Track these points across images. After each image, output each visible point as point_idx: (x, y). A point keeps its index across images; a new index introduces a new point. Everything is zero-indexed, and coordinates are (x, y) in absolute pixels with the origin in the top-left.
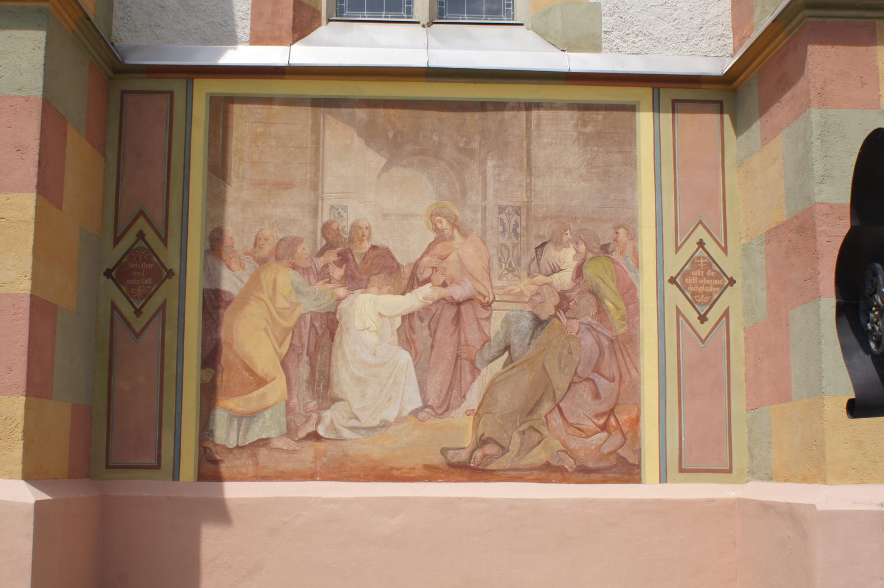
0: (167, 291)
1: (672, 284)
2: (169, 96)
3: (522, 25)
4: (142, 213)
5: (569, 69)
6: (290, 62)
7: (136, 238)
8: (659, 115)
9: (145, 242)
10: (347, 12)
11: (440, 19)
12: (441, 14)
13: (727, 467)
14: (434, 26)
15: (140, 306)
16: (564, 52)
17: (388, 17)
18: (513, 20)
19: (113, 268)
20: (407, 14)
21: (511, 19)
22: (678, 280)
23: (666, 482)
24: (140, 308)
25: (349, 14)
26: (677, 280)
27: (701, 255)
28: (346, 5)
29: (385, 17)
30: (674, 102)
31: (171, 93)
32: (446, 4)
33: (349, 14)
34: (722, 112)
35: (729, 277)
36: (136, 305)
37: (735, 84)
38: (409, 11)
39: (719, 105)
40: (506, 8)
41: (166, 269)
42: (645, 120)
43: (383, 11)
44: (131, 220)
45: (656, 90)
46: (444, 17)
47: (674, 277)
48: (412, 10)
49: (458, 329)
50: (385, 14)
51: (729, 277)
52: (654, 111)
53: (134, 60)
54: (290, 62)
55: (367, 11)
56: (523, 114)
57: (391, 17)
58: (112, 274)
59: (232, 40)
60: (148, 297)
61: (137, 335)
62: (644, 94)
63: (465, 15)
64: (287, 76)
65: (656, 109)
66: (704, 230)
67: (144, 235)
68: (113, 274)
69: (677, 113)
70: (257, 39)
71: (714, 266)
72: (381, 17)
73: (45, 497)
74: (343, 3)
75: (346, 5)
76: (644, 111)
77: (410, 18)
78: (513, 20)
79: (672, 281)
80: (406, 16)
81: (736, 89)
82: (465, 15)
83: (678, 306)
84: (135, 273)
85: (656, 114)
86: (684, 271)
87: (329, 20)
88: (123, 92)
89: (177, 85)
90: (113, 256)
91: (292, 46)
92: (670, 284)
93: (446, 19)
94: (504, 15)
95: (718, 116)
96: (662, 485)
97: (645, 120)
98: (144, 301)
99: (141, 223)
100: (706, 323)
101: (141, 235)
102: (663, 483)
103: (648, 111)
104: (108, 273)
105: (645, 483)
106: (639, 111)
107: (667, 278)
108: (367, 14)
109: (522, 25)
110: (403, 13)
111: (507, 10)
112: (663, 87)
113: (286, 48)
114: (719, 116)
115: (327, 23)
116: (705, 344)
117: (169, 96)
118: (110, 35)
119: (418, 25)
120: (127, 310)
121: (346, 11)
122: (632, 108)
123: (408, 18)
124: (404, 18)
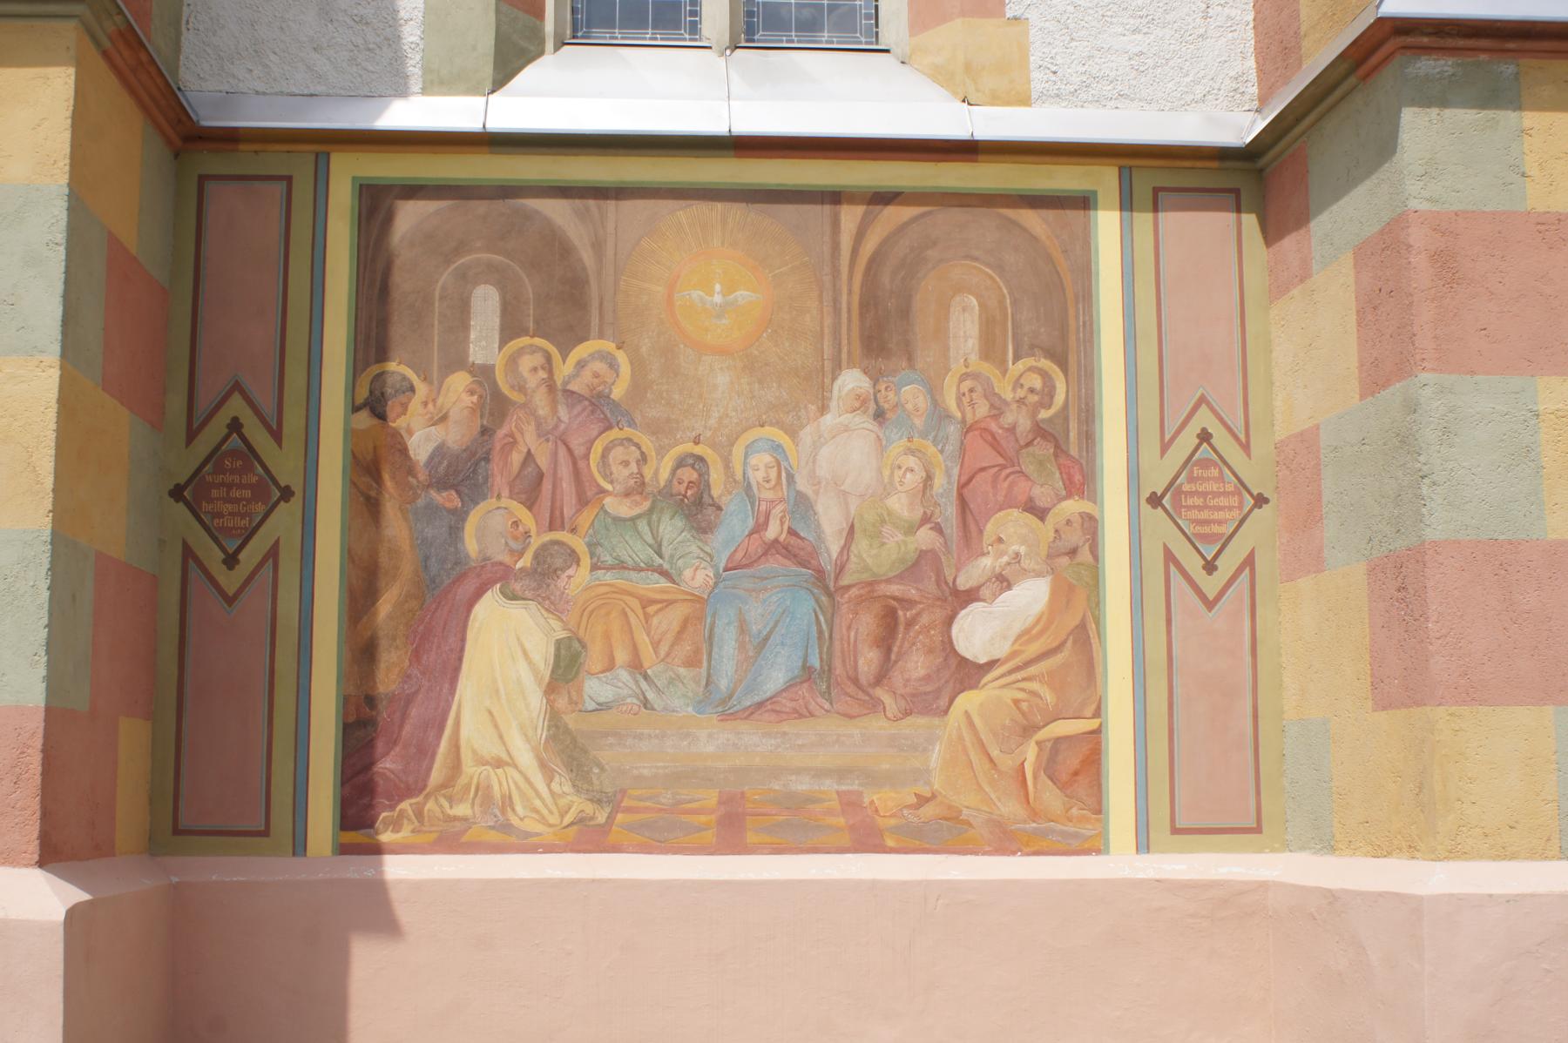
0: (283, 522)
1: (1155, 507)
2: (285, 183)
3: (887, 51)
4: (237, 387)
5: (484, 126)
7: (1197, 441)
8: (1132, 215)
9: (1211, 445)
10: (761, 33)
12: (750, 31)
17: (656, 39)
18: (877, 43)
19: (185, 483)
20: (690, 34)
21: (874, 40)
25: (764, 35)
26: (1252, 502)
27: (1205, 456)
28: (582, 17)
29: (651, 39)
32: (758, 14)
33: (764, 35)
34: (1239, 210)
37: (1262, 162)
38: (694, 28)
39: (1234, 195)
40: (688, 19)
41: (276, 483)
42: (1107, 223)
43: (822, 31)
45: (1126, 173)
47: (183, 483)
48: (699, 26)
49: (951, 585)
50: (652, 34)
52: (1121, 209)
53: (211, 119)
54: (487, 126)
56: (827, 208)
57: (662, 39)
58: (185, 494)
61: (230, 600)
62: (1105, 179)
63: (793, 34)
64: (980, 157)
65: (1127, 204)
66: (1210, 414)
67: (241, 426)
68: (1166, 501)
69: (1162, 211)
70: (438, 83)
71: (1228, 476)
72: (645, 39)
74: (754, 17)
77: (695, 40)
78: (877, 43)
79: (287, 494)
81: (1261, 170)
83: (1170, 546)
84: (215, 493)
85: (1126, 214)
86: (1175, 485)
87: (560, 43)
88: (203, 179)
89: (300, 167)
90: (184, 465)
91: (490, 96)
92: (1149, 506)
94: (685, 31)
95: (1233, 216)
97: (1107, 223)
99: (236, 406)
100: (1215, 573)
101: (235, 426)
104: (177, 493)
106: (1096, 209)
107: (1146, 494)
108: (620, 33)
109: (710, 48)
110: (683, 32)
115: (557, 49)
116: (1213, 611)
117: (285, 183)
118: (175, 71)
119: (888, 54)
120: (212, 556)
121: (758, 32)
122: (1084, 202)
123: (691, 40)
124: (685, 40)
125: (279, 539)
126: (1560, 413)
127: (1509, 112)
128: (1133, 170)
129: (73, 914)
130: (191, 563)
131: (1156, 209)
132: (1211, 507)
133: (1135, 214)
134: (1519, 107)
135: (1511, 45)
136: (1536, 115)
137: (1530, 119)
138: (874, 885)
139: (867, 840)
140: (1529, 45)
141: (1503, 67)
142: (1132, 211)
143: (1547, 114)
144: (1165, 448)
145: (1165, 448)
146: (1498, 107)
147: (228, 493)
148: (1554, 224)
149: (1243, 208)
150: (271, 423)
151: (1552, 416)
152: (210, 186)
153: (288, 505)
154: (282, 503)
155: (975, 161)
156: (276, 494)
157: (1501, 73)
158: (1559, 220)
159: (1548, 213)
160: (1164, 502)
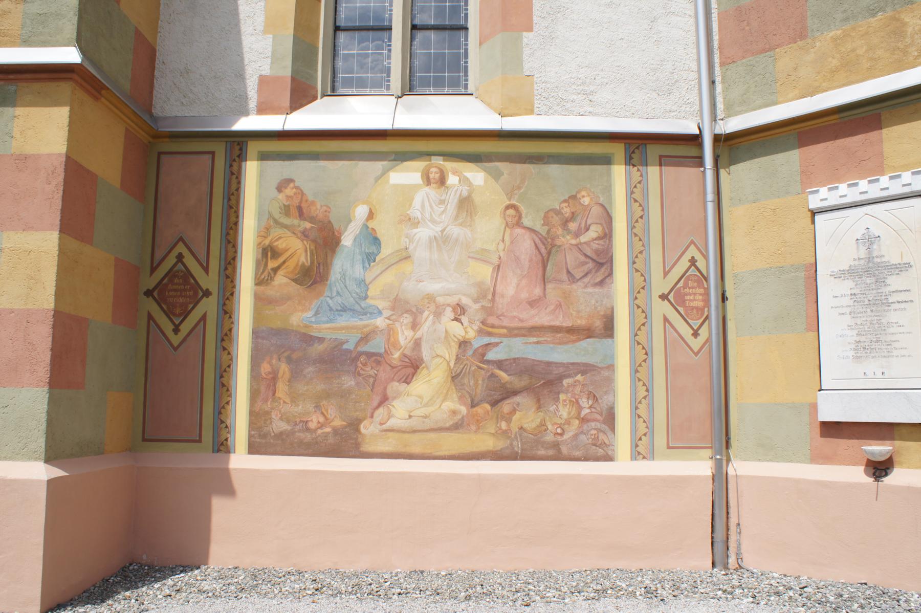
1: (663, 300)
3: (472, 94)
6: (503, 128)
11: (410, 92)
13: (672, 444)
14: (405, 96)
15: (179, 322)
16: (541, 116)
22: (671, 297)
23: (653, 459)
24: (697, 329)
28: (416, 83)
30: (661, 157)
31: (213, 153)
35: (204, 289)
36: (175, 321)
38: (466, 87)
40: (386, 83)
42: (619, 171)
43: (445, 87)
44: (164, 254)
46: (415, 91)
51: (204, 289)
52: (626, 165)
55: (448, 87)
59: (245, 113)
60: (186, 314)
62: (618, 150)
63: (432, 88)
64: (388, 138)
68: (155, 294)
70: (263, 109)
73: (58, 473)
75: (416, 83)
76: (617, 164)
77: (467, 92)
79: (664, 297)
80: (463, 90)
82: (432, 88)
87: (323, 95)
88: (160, 154)
91: (288, 115)
93: (416, 92)
96: (634, 462)
98: (182, 318)
102: (633, 460)
103: (656, 166)
105: (617, 461)
106: (614, 164)
109: (472, 94)
111: (387, 85)
112: (650, 144)
113: (284, 116)
114: (658, 168)
115: (322, 97)
125: (664, 315)
126: (12, 249)
127: (10, 108)
128: (647, 145)
129: (52, 483)
130: (202, 323)
131: (661, 165)
132: (696, 300)
133: (649, 168)
134: (14, 105)
135: (11, 77)
136: (22, 109)
137: (19, 111)
138: (598, 477)
139: (558, 457)
140: (19, 76)
141: (10, 87)
142: (647, 166)
143: (27, 108)
144: (666, 274)
145: (666, 274)
146: (5, 106)
147: (694, 297)
148: (22, 160)
149: (648, 164)
150: (203, 263)
151: (8, 250)
152: (162, 157)
153: (207, 299)
154: (205, 298)
155: (386, 139)
156: (671, 297)
157: (9, 90)
158: (26, 158)
159: (21, 154)
160: (669, 297)
